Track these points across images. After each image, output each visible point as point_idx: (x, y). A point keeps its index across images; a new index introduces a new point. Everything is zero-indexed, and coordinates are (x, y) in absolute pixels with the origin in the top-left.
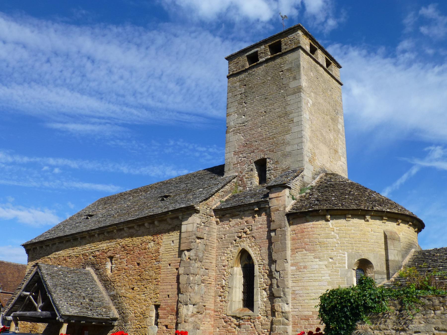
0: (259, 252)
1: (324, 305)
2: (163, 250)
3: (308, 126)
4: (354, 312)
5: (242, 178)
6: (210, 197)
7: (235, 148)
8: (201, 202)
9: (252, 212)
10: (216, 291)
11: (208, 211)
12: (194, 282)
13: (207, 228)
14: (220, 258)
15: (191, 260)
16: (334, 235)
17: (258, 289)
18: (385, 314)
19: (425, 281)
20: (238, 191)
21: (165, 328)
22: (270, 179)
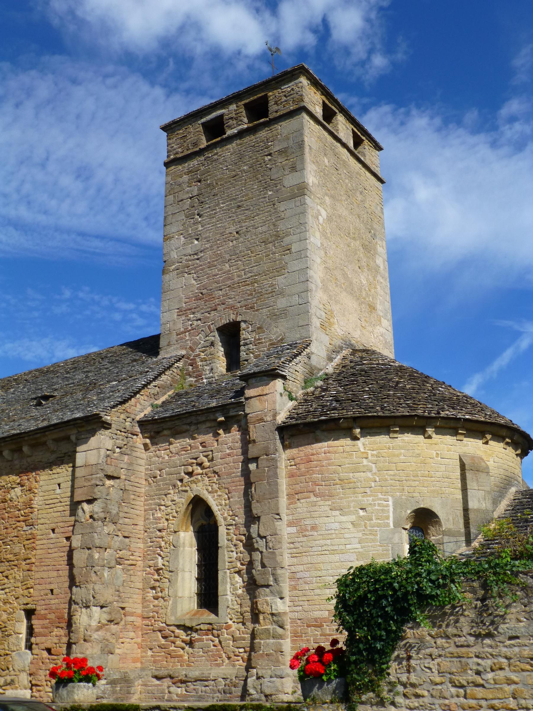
0: (227, 502)
1: (344, 596)
2: (41, 503)
3: (318, 260)
4: (399, 606)
5: (194, 359)
6: (132, 397)
7: (180, 301)
8: (113, 407)
9: (213, 424)
10: (144, 579)
11: (127, 424)
12: (101, 563)
13: (126, 457)
14: (153, 514)
15: (94, 520)
16: (367, 465)
17: (225, 573)
18: (457, 607)
19: (527, 543)
20: (186, 386)
21: (45, 654)
22: (247, 360)
